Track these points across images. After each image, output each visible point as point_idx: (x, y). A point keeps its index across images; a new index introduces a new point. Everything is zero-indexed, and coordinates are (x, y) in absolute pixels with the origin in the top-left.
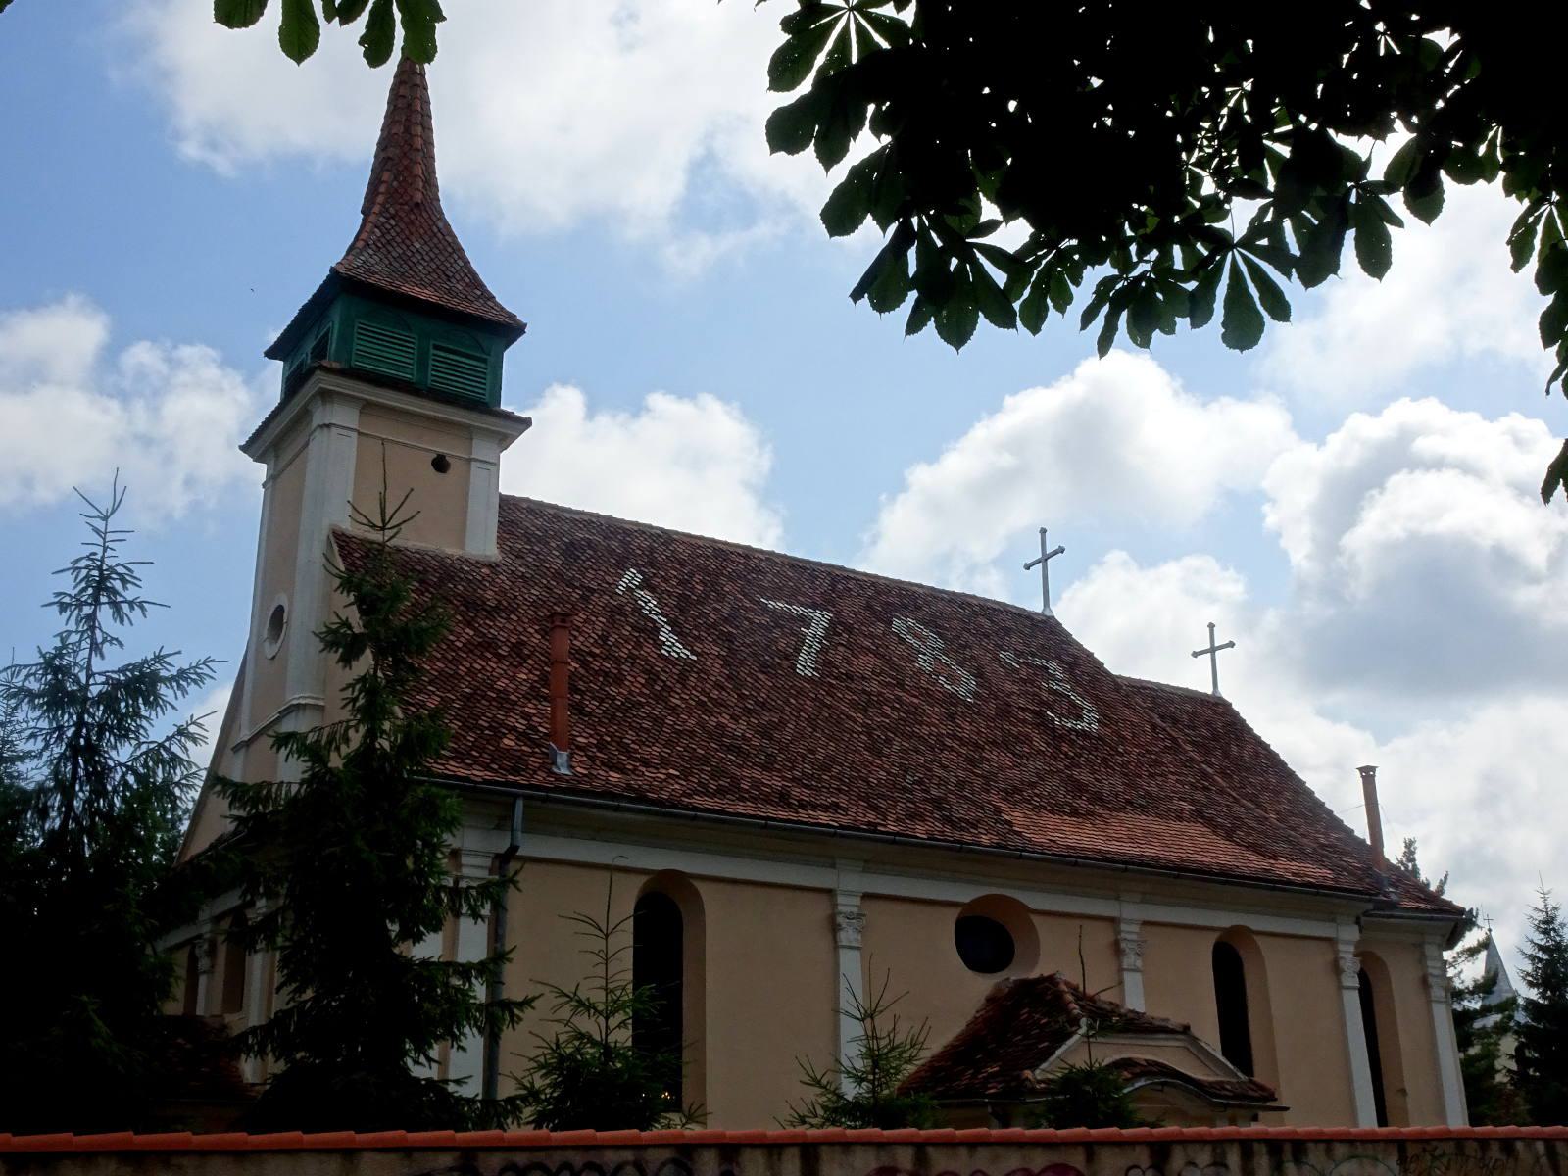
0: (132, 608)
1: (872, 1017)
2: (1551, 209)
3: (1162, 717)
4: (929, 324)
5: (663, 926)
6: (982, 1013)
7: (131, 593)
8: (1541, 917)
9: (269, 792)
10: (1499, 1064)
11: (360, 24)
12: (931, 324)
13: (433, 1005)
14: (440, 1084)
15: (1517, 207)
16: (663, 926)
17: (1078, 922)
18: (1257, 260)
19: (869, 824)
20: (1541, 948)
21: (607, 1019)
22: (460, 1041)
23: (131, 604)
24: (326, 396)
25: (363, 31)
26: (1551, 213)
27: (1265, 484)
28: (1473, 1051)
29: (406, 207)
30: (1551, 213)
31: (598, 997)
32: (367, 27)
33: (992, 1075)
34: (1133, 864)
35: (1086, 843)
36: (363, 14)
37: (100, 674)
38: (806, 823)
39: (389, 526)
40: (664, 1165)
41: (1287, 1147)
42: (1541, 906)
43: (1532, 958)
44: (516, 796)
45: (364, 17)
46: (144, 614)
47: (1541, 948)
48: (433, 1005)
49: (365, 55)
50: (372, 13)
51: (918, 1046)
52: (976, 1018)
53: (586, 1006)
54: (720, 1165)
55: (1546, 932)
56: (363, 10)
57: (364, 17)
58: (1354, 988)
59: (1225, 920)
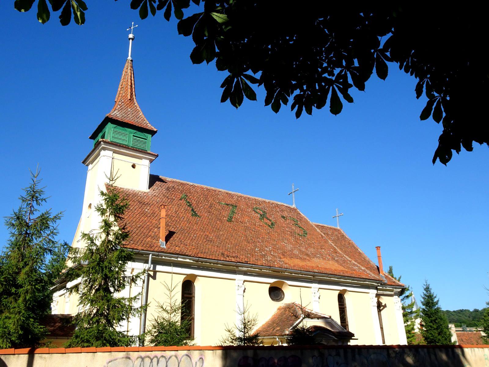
0: (42, 201)
1: (244, 314)
2: (427, 80)
3: (324, 234)
4: (228, 99)
5: (188, 287)
6: (276, 313)
7: (43, 196)
8: (425, 287)
9: (79, 250)
10: (415, 327)
11: (59, 12)
12: (229, 99)
13: (122, 310)
14: (123, 333)
15: (418, 80)
16: (188, 287)
17: (300, 288)
18: (337, 84)
19: (245, 261)
20: (425, 295)
21: (170, 314)
22: (120, 322)
23: (42, 200)
24: (104, 149)
25: (60, 14)
26: (427, 80)
27: (441, 307)
28: (409, 323)
29: (127, 100)
30: (427, 80)
31: (169, 308)
32: (62, 13)
33: (278, 330)
34: (316, 273)
35: (328, 266)
36: (61, 9)
37: (32, 220)
38: (228, 261)
39: (113, 180)
40: (183, 356)
41: (357, 350)
42: (425, 284)
43: (424, 298)
44: (150, 254)
45: (61, 10)
46: (46, 201)
47: (425, 295)
48: (122, 310)
49: (61, 21)
50: (64, 9)
51: (255, 321)
52: (274, 314)
53: (165, 310)
54: (199, 356)
55: (427, 291)
56: (61, 8)
57: (61, 10)
58: (376, 306)
59: (341, 288)
